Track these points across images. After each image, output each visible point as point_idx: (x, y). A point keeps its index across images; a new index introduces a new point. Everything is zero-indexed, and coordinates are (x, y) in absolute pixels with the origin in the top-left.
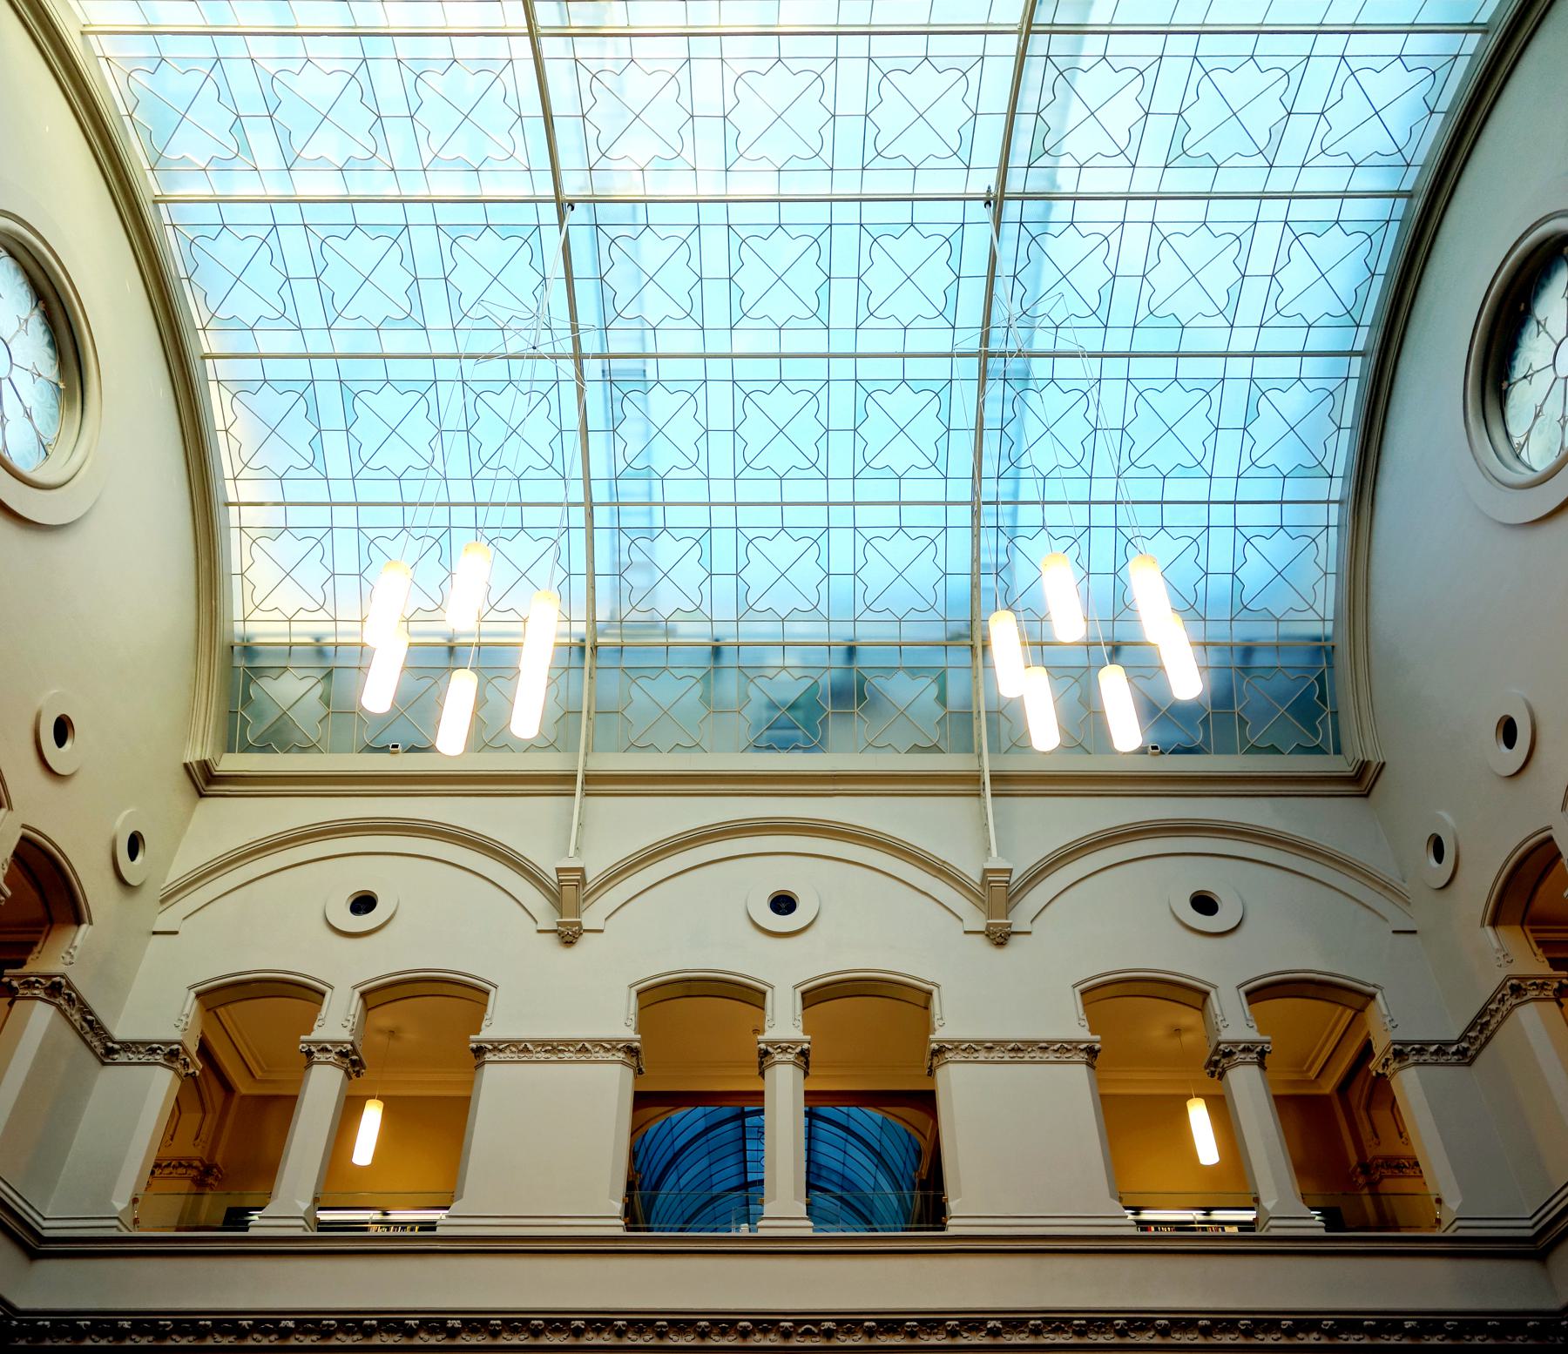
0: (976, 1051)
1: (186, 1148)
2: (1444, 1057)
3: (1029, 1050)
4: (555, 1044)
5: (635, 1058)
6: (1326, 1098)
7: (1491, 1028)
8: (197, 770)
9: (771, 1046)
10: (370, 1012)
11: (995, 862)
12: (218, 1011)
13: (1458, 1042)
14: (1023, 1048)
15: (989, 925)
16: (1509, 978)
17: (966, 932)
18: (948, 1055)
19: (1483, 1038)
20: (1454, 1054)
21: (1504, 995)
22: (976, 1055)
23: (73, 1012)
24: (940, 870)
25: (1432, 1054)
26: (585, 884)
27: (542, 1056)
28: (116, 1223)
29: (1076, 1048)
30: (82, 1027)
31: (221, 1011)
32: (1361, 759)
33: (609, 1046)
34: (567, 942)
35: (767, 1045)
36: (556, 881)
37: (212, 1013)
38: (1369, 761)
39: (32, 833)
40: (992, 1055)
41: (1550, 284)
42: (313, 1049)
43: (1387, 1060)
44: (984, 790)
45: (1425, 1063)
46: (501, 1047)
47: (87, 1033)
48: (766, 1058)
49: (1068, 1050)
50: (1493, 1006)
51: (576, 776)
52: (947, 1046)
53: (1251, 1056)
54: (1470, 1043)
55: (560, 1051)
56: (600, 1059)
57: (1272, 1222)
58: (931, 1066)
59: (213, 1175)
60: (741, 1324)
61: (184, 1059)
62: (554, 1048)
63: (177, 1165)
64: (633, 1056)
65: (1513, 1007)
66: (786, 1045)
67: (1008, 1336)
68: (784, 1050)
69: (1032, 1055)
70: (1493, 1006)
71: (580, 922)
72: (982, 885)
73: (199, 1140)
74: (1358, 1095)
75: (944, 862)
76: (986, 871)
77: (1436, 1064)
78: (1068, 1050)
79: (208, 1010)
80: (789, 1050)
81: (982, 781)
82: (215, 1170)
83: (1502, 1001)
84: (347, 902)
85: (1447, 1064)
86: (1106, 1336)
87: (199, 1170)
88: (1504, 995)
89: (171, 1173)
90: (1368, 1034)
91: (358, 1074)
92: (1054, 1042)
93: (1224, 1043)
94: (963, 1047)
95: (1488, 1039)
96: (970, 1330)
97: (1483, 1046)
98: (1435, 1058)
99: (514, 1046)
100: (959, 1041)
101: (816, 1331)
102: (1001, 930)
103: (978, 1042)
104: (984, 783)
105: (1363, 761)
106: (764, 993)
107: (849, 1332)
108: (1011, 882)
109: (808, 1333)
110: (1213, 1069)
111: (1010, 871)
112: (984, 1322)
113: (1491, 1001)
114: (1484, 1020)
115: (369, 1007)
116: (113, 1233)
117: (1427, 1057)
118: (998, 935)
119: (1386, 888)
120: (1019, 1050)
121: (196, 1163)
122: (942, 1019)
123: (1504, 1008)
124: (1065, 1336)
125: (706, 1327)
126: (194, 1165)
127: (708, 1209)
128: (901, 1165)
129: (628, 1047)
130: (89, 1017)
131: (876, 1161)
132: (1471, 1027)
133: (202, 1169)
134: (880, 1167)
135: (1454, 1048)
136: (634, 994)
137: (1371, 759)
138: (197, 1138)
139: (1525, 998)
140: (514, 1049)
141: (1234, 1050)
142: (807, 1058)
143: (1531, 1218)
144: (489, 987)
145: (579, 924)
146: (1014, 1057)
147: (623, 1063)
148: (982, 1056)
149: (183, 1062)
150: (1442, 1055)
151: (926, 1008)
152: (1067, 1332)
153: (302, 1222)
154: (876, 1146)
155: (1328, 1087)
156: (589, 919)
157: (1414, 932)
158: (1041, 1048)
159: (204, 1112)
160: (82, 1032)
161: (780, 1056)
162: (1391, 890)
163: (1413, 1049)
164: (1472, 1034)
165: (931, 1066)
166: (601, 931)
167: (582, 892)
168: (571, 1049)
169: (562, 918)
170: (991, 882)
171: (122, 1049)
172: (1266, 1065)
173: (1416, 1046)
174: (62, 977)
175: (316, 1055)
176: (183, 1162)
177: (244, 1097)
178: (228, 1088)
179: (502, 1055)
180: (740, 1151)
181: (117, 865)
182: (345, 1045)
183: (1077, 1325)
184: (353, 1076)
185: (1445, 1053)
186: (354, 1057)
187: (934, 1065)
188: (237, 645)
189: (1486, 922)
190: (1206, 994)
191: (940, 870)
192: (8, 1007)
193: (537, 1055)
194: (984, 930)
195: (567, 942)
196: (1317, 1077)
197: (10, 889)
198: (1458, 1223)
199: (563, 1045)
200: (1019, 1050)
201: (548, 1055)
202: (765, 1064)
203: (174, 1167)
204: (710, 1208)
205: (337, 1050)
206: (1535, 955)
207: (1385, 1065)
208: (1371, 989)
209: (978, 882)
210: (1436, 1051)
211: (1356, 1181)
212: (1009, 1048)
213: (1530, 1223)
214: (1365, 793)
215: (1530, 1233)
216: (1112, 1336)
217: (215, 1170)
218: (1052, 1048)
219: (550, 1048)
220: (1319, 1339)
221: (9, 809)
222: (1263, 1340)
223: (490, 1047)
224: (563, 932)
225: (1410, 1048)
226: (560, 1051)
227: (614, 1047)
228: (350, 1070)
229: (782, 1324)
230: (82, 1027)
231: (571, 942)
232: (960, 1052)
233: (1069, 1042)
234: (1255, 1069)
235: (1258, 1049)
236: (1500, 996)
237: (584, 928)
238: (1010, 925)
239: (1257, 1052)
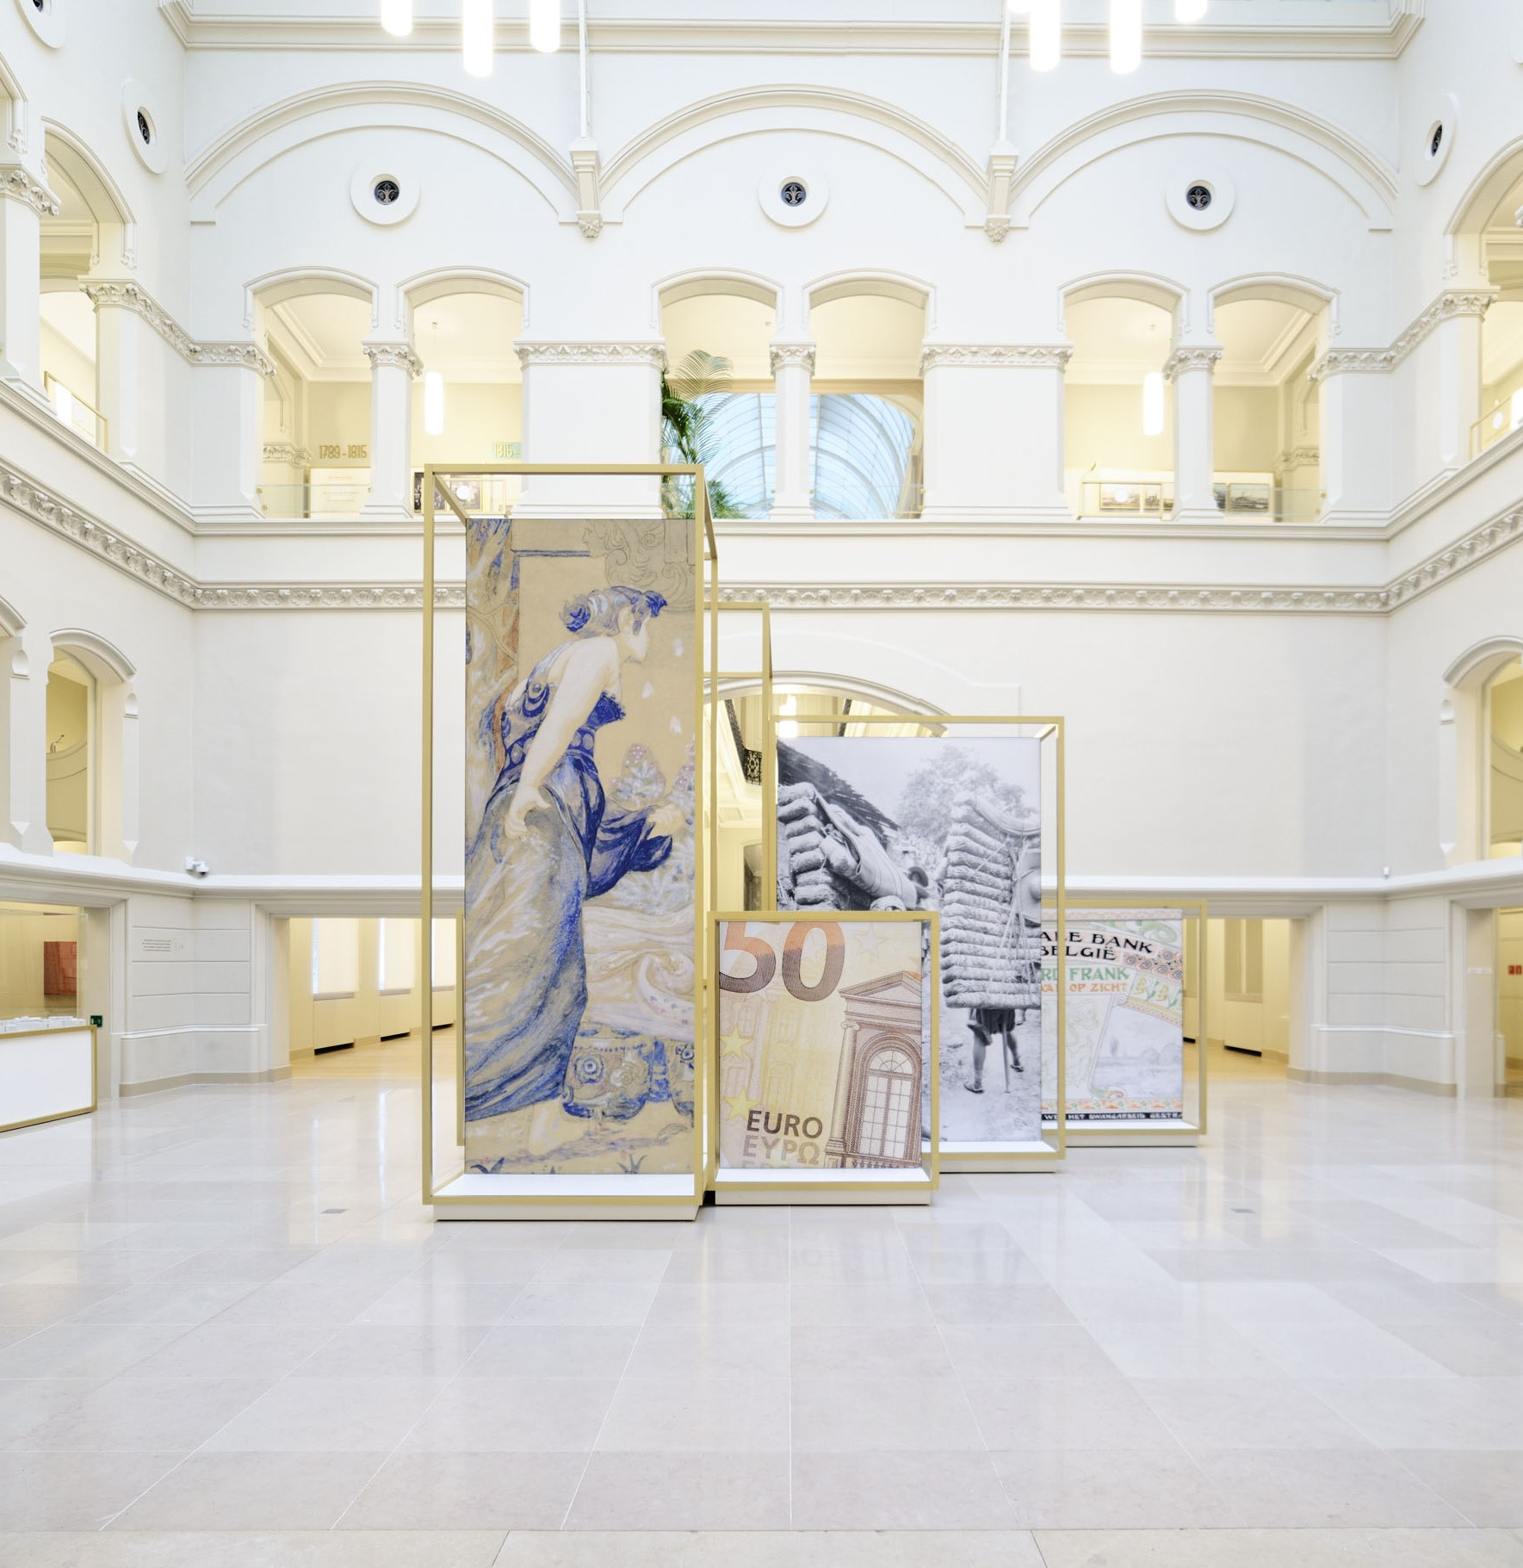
0: (963, 355)
2: (1372, 365)
4: (589, 346)
5: (661, 360)
6: (1274, 389)
7: (1417, 340)
8: (169, 10)
12: (275, 307)
15: (988, 221)
16: (1445, 293)
18: (937, 359)
20: (1381, 361)
25: (1362, 361)
27: (580, 358)
28: (250, 511)
29: (1050, 353)
31: (278, 308)
32: (1403, 12)
33: (637, 349)
34: (589, 237)
36: (572, 166)
37: (269, 310)
38: (1410, 15)
39: (62, 131)
40: (976, 359)
41: (791, 811)
43: (1322, 366)
45: (1353, 371)
46: (541, 349)
47: (170, 336)
48: (778, 361)
50: (1424, 319)
52: (937, 350)
53: (1203, 362)
54: (1397, 352)
55: (594, 353)
57: (1183, 513)
58: (922, 368)
59: (304, 458)
61: (261, 360)
65: (1441, 321)
68: (793, 353)
70: (1424, 319)
74: (1301, 386)
76: (992, 157)
77: (1363, 371)
79: (267, 307)
84: (371, 183)
85: (1373, 371)
86: (1035, 602)
88: (1437, 309)
89: (269, 457)
92: (1031, 347)
93: (1182, 349)
94: (951, 351)
95: (1412, 349)
100: (948, 346)
103: (964, 347)
107: (840, 597)
109: (808, 597)
110: (1169, 372)
111: (1016, 158)
112: (943, 590)
114: (1415, 331)
115: (414, 305)
119: (1378, 178)
121: (288, 448)
123: (1433, 322)
125: (731, 594)
127: (729, 471)
130: (168, 322)
131: (877, 431)
134: (881, 436)
135: (1382, 356)
136: (656, 294)
137: (1413, 12)
138: (282, 425)
139: (1454, 314)
140: (553, 351)
142: (813, 361)
144: (523, 287)
145: (599, 217)
146: (994, 362)
147: (652, 365)
148: (968, 359)
152: (1005, 598)
153: (402, 510)
154: (878, 417)
155: (1278, 380)
156: (609, 211)
158: (1020, 353)
159: (282, 400)
160: (166, 336)
161: (789, 358)
162: (1383, 183)
164: (1401, 344)
165: (922, 368)
166: (621, 223)
167: (598, 179)
168: (604, 351)
169: (581, 209)
170: (995, 171)
171: (203, 349)
173: (1350, 354)
176: (277, 448)
177: (310, 383)
178: (296, 377)
179: (543, 357)
180: (756, 418)
181: (138, 153)
182: (402, 347)
184: (414, 375)
187: (925, 368)
188: (935, 1147)
189: (1449, 231)
190: (1178, 297)
193: (574, 357)
194: (983, 224)
195: (589, 237)
196: (1272, 369)
199: (597, 347)
201: (584, 357)
205: (397, 351)
206: (1481, 267)
207: (1319, 371)
209: (984, 169)
210: (1366, 358)
212: (992, 352)
213: (1388, 515)
214: (1395, 56)
215: (1384, 524)
216: (1039, 601)
219: (585, 350)
223: (531, 349)
225: (1344, 356)
226: (594, 353)
227: (642, 350)
229: (789, 591)
235: (1211, 356)
237: (605, 220)
238: (1008, 221)
239: (1210, 359)
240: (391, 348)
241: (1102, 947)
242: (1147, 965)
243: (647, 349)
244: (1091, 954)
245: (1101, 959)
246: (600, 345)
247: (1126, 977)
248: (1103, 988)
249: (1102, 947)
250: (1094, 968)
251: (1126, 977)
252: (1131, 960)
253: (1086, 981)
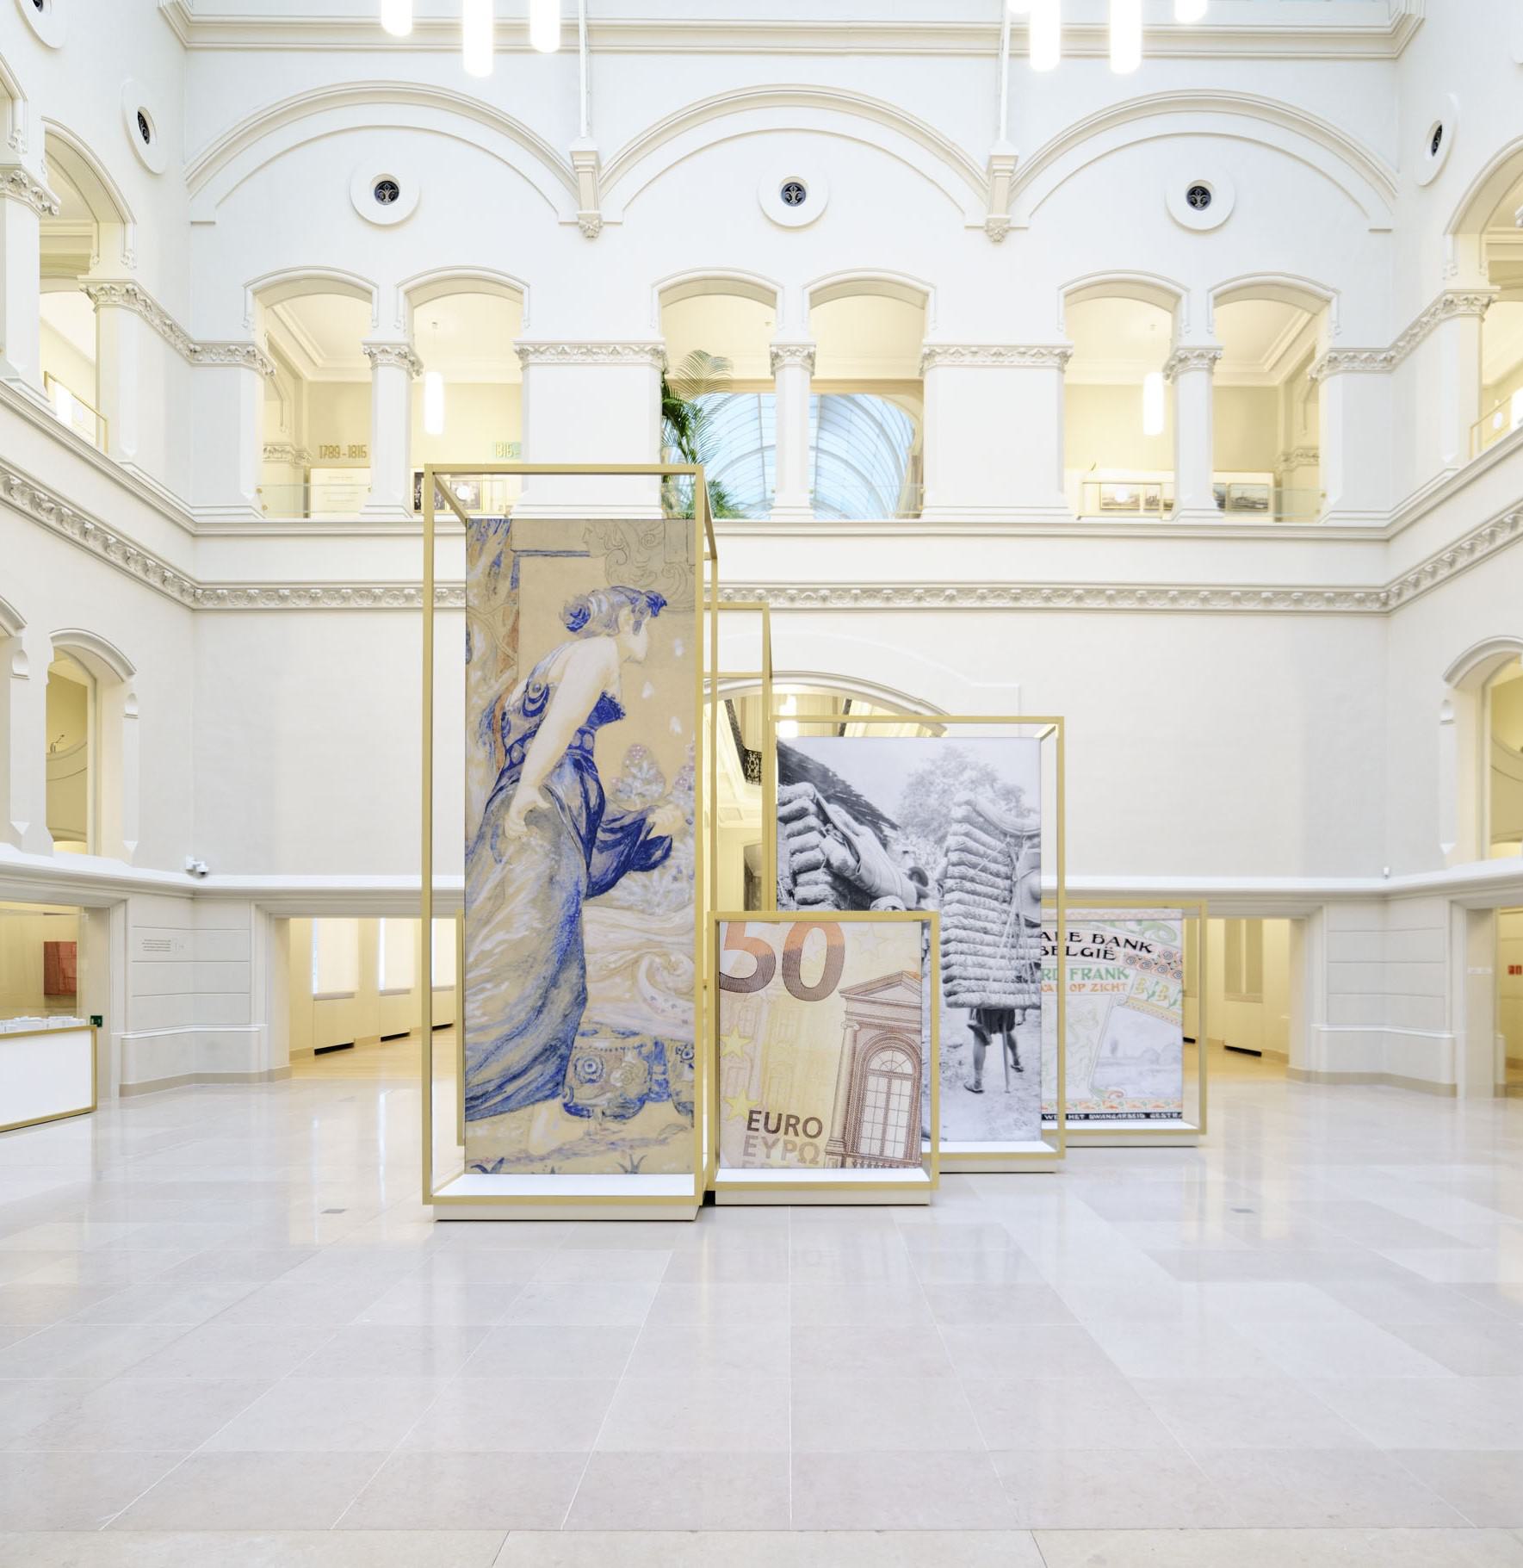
0: (963, 355)
1: (283, 437)
3: (1009, 354)
6: (1274, 389)
10: (416, 310)
15: (988, 221)
18: (937, 359)
19: (1408, 348)
20: (1381, 361)
21: (1437, 309)
22: (962, 359)
23: (153, 317)
24: (949, 153)
27: (580, 358)
28: (250, 510)
29: (1051, 353)
30: (164, 331)
31: (278, 308)
32: (1403, 13)
33: (637, 349)
35: (777, 349)
37: (269, 309)
42: (375, 351)
45: (1354, 371)
46: (542, 349)
48: (778, 361)
49: (1043, 355)
50: (1424, 319)
51: (578, 25)
55: (594, 353)
57: (1182, 513)
60: (758, 591)
61: (261, 360)
62: (588, 350)
65: (1441, 321)
67: (960, 601)
68: (793, 353)
70: (1424, 319)
72: (988, 172)
75: (954, 144)
76: (992, 157)
77: (1364, 371)
78: (1043, 355)
79: (267, 307)
80: (798, 353)
81: (1001, 38)
83: (1434, 314)
87: (293, 455)
88: (1437, 309)
89: (269, 457)
90: (1316, 339)
91: (418, 372)
92: (1031, 347)
94: (951, 351)
95: (1412, 349)
100: (948, 346)
101: (815, 596)
104: (1003, 41)
105: (1404, 14)
106: (775, 294)
107: (840, 597)
109: (808, 597)
111: (1016, 158)
112: (943, 590)
113: (1424, 315)
114: (1414, 331)
115: (414, 305)
116: (252, 519)
117: (1356, 364)
119: (1378, 178)
121: (288, 448)
131: (877, 431)
134: (881, 437)
135: (1383, 356)
137: (1413, 12)
138: (282, 425)
140: (553, 352)
141: (1189, 356)
142: (813, 361)
143: (1390, 512)
144: (523, 287)
145: (599, 217)
146: (994, 362)
149: (260, 362)
150: (1371, 363)
151: (923, 308)
153: (401, 510)
155: (1278, 380)
157: (1389, 231)
158: (1020, 353)
162: (1383, 183)
164: (1401, 344)
168: (604, 350)
171: (203, 349)
172: (1215, 371)
174: (134, 284)
175: (379, 356)
176: (277, 447)
177: (311, 384)
178: (296, 376)
179: (543, 357)
180: (756, 419)
182: (403, 347)
183: (1013, 594)
184: (414, 374)
189: (1449, 231)
190: (1178, 297)
192: (94, 315)
195: (589, 237)
196: (1272, 369)
201: (584, 357)
202: (777, 366)
203: (270, 451)
205: (397, 351)
206: (1481, 267)
207: (1319, 371)
209: (984, 169)
210: (1366, 359)
211: (1277, 468)
212: (992, 352)
213: (1387, 516)
214: (1395, 56)
218: (1029, 353)
219: (585, 350)
221: (24, 101)
222: (1152, 605)
223: (531, 349)
224: (584, 226)
226: (594, 353)
227: (642, 350)
228: (411, 370)
230: (164, 331)
231: (593, 237)
232: (948, 356)
233: (1046, 347)
234: (1204, 374)
235: (1211, 356)
236: (1433, 310)
237: (604, 220)
238: (1009, 221)
240: (391, 348)
241: (1102, 947)
242: (1147, 965)
244: (1091, 954)
245: (1101, 959)
246: (600, 345)
248: (1103, 988)
249: (1102, 947)
250: (1094, 968)
251: (1126, 977)
252: (1131, 960)
253: (1086, 981)
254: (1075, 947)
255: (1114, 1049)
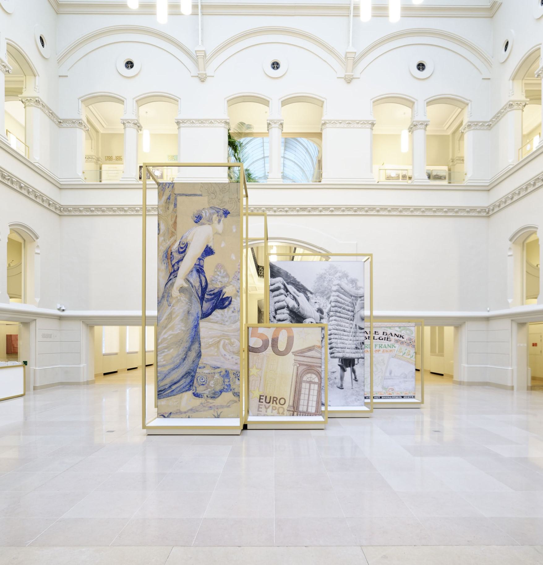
1: (92, 153)
6: (448, 136)
7: (500, 118)
9: (271, 121)
11: (351, 49)
12: (89, 107)
13: (489, 122)
14: (351, 123)
15: (345, 76)
16: (510, 101)
17: (338, 78)
18: (327, 125)
19: (496, 121)
22: (336, 125)
26: (206, 56)
27: (199, 125)
28: (80, 180)
29: (368, 123)
30: (49, 115)
33: (219, 121)
34: (202, 81)
37: (87, 107)
43: (465, 128)
44: (350, 14)
45: (477, 129)
46: (185, 122)
47: (51, 117)
49: (365, 124)
50: (502, 111)
55: (204, 123)
56: (217, 126)
57: (415, 181)
61: (84, 125)
63: (88, 158)
64: (227, 125)
66: (276, 121)
67: (335, 212)
68: (275, 123)
69: (354, 125)
71: (206, 73)
73: (175, 215)
74: (458, 135)
75: (333, 48)
76: (347, 53)
79: (86, 106)
80: (277, 123)
82: (100, 159)
83: (506, 109)
87: (95, 159)
88: (506, 107)
89: (87, 160)
90: (463, 118)
91: (141, 130)
92: (361, 121)
95: (498, 122)
96: (325, 210)
97: (496, 124)
98: (480, 127)
99: (189, 121)
101: (283, 210)
102: (349, 78)
103: (337, 121)
106: (269, 102)
107: (292, 211)
108: (355, 58)
109: (281, 211)
110: (410, 130)
112: (329, 208)
115: (139, 105)
118: (348, 79)
119: (486, 60)
120: (350, 123)
121: (94, 157)
122: (326, 112)
124: (351, 212)
126: (94, 158)
128: (313, 153)
129: (225, 122)
131: (306, 151)
132: (494, 118)
133: (96, 159)
134: (307, 153)
135: (487, 124)
138: (92, 149)
140: (189, 122)
142: (282, 126)
143: (489, 180)
145: (206, 74)
146: (348, 126)
148: (338, 125)
151: (322, 107)
152: (352, 211)
155: (450, 132)
156: (209, 72)
159: (92, 140)
160: (50, 117)
163: (474, 124)
168: (207, 122)
169: (199, 71)
170: (348, 57)
171: (63, 122)
175: (126, 124)
177: (102, 134)
178: (97, 131)
179: (186, 124)
180: (262, 146)
184: (139, 131)
185: (484, 125)
186: (138, 125)
187: (323, 128)
189: (511, 79)
190: (414, 103)
191: (331, 51)
195: (202, 81)
196: (447, 129)
197: (12, 67)
198: (469, 181)
200: (350, 123)
201: (200, 124)
202: (269, 128)
203: (87, 158)
204: (253, 165)
207: (464, 129)
208: (468, 102)
209: (344, 57)
210: (481, 125)
212: (347, 123)
213: (489, 181)
215: (488, 184)
217: (100, 159)
220: (419, 213)
226: (204, 123)
227: (221, 122)
231: (203, 81)
237: (207, 75)
238: (353, 76)
239: (425, 125)
241: (386, 336)
242: (402, 343)
243: (223, 121)
244: (382, 339)
245: (386, 341)
247: (395, 347)
248: (387, 351)
249: (386, 336)
250: (383, 344)
251: (395, 347)
252: (397, 341)
253: (380, 349)
254: (377, 337)
255: (391, 373)
